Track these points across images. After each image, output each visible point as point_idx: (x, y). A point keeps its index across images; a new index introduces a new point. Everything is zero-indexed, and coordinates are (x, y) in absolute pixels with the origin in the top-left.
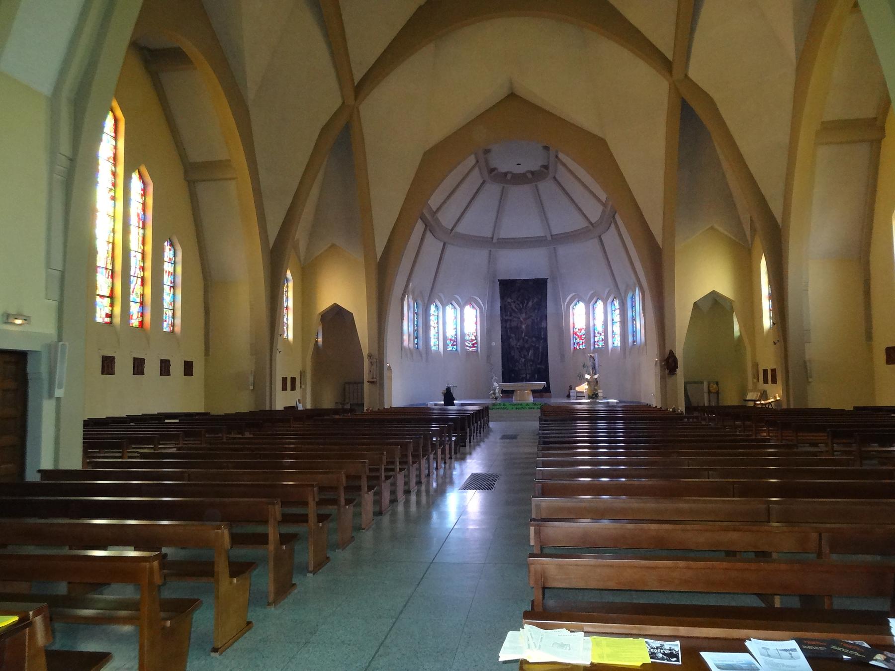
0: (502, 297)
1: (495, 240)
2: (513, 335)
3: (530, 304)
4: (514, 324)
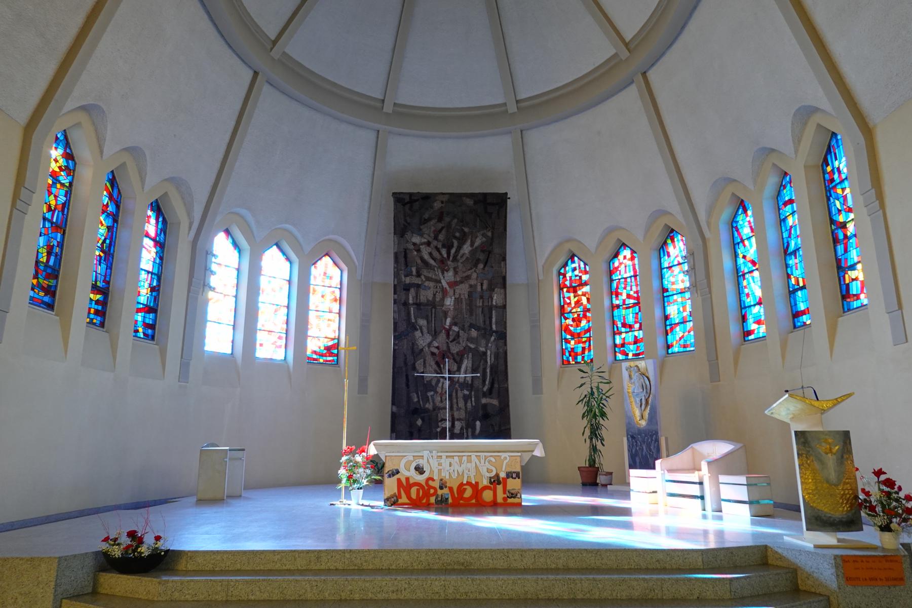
0: (401, 230)
1: (388, 108)
2: (422, 322)
3: (466, 249)
4: (426, 295)
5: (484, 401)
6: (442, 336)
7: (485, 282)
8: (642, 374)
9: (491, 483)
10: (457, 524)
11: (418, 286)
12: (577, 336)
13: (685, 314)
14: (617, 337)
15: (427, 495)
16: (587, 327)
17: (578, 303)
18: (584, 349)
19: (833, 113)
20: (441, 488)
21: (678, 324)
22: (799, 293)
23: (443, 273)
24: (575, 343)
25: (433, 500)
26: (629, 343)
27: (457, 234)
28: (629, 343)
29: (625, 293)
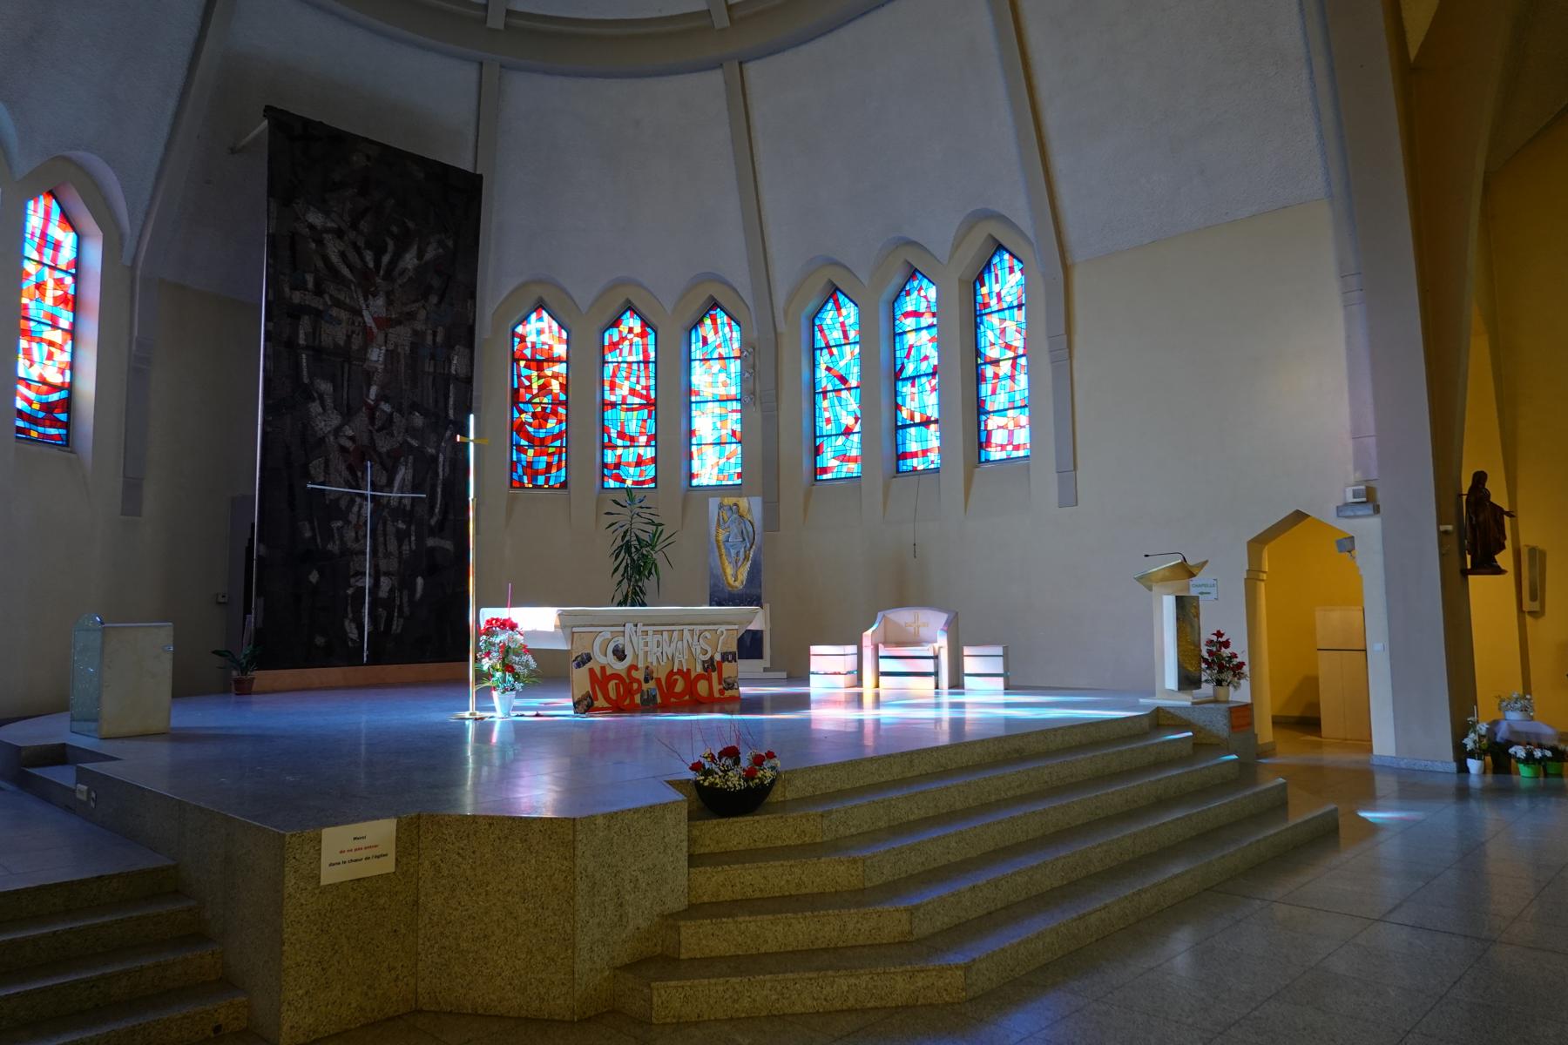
2: (325, 387)
3: (410, 260)
4: (333, 334)
5: (431, 542)
6: (361, 419)
7: (440, 330)
9: (705, 669)
10: (463, 751)
11: (318, 315)
12: (540, 444)
13: (723, 432)
14: (608, 453)
15: (630, 692)
16: (556, 431)
17: (544, 389)
18: (549, 465)
19: (1030, 234)
20: (646, 681)
22: (913, 430)
23: (366, 299)
24: (536, 455)
25: (637, 699)
26: (628, 464)
27: (395, 229)
28: (628, 464)
29: (626, 385)
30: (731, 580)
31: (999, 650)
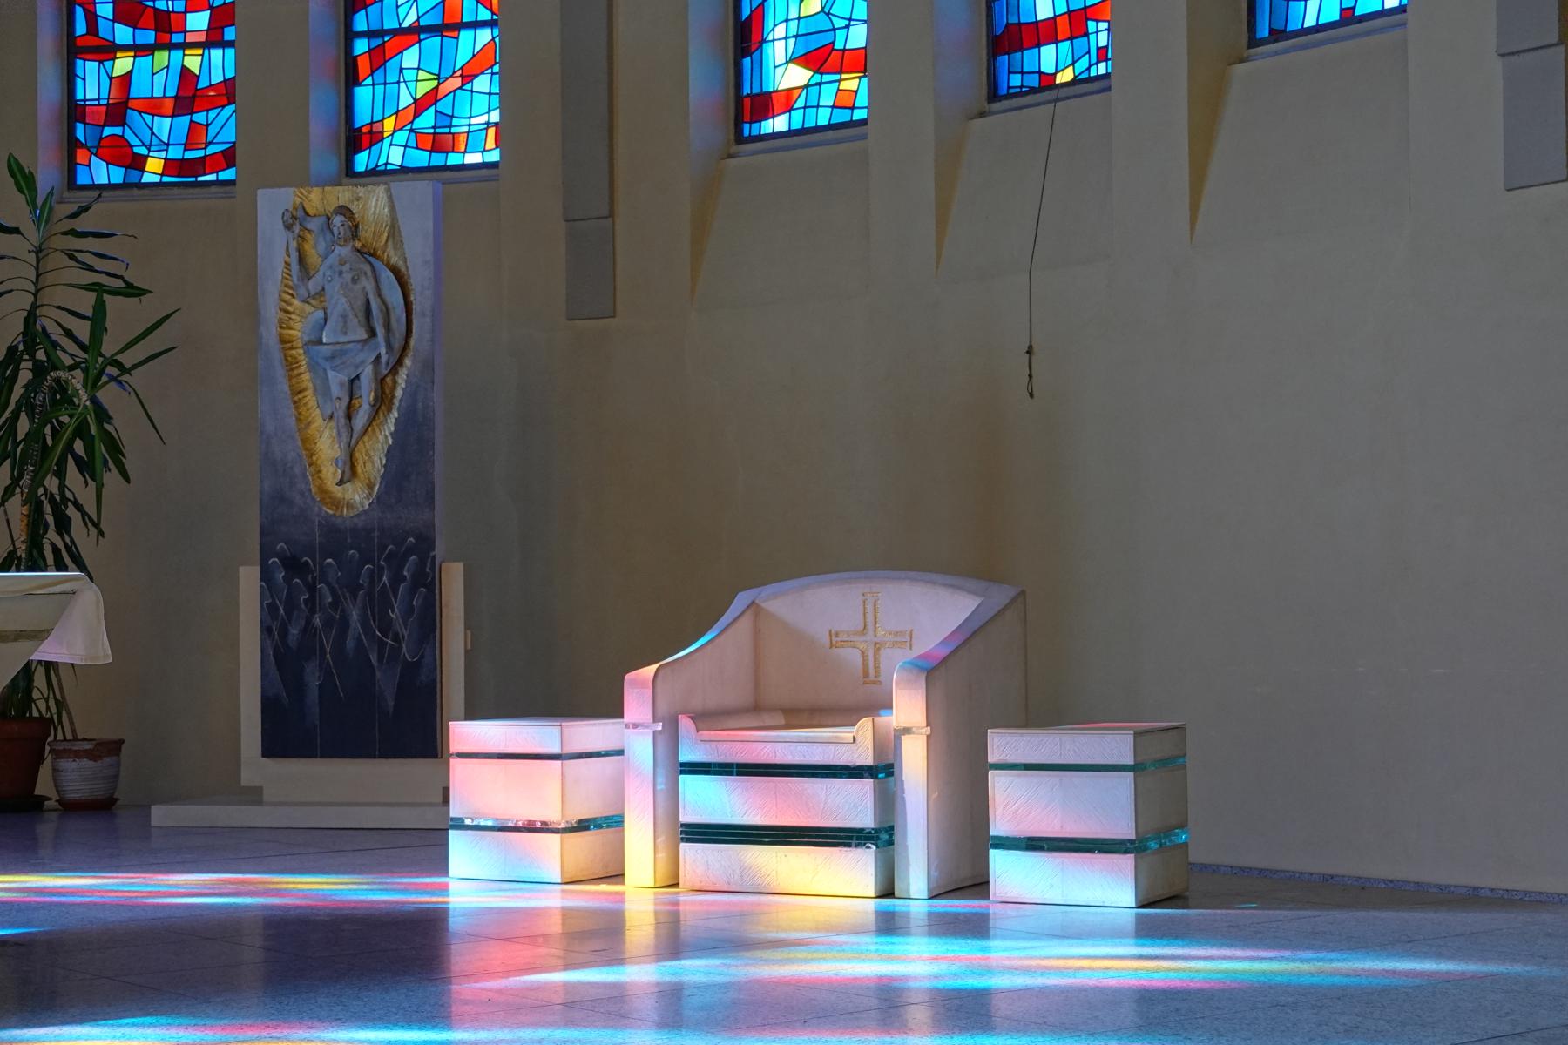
8: (367, 253)
21: (415, 33)
26: (153, 106)
28: (153, 106)
30: (330, 474)
31: (1118, 745)
